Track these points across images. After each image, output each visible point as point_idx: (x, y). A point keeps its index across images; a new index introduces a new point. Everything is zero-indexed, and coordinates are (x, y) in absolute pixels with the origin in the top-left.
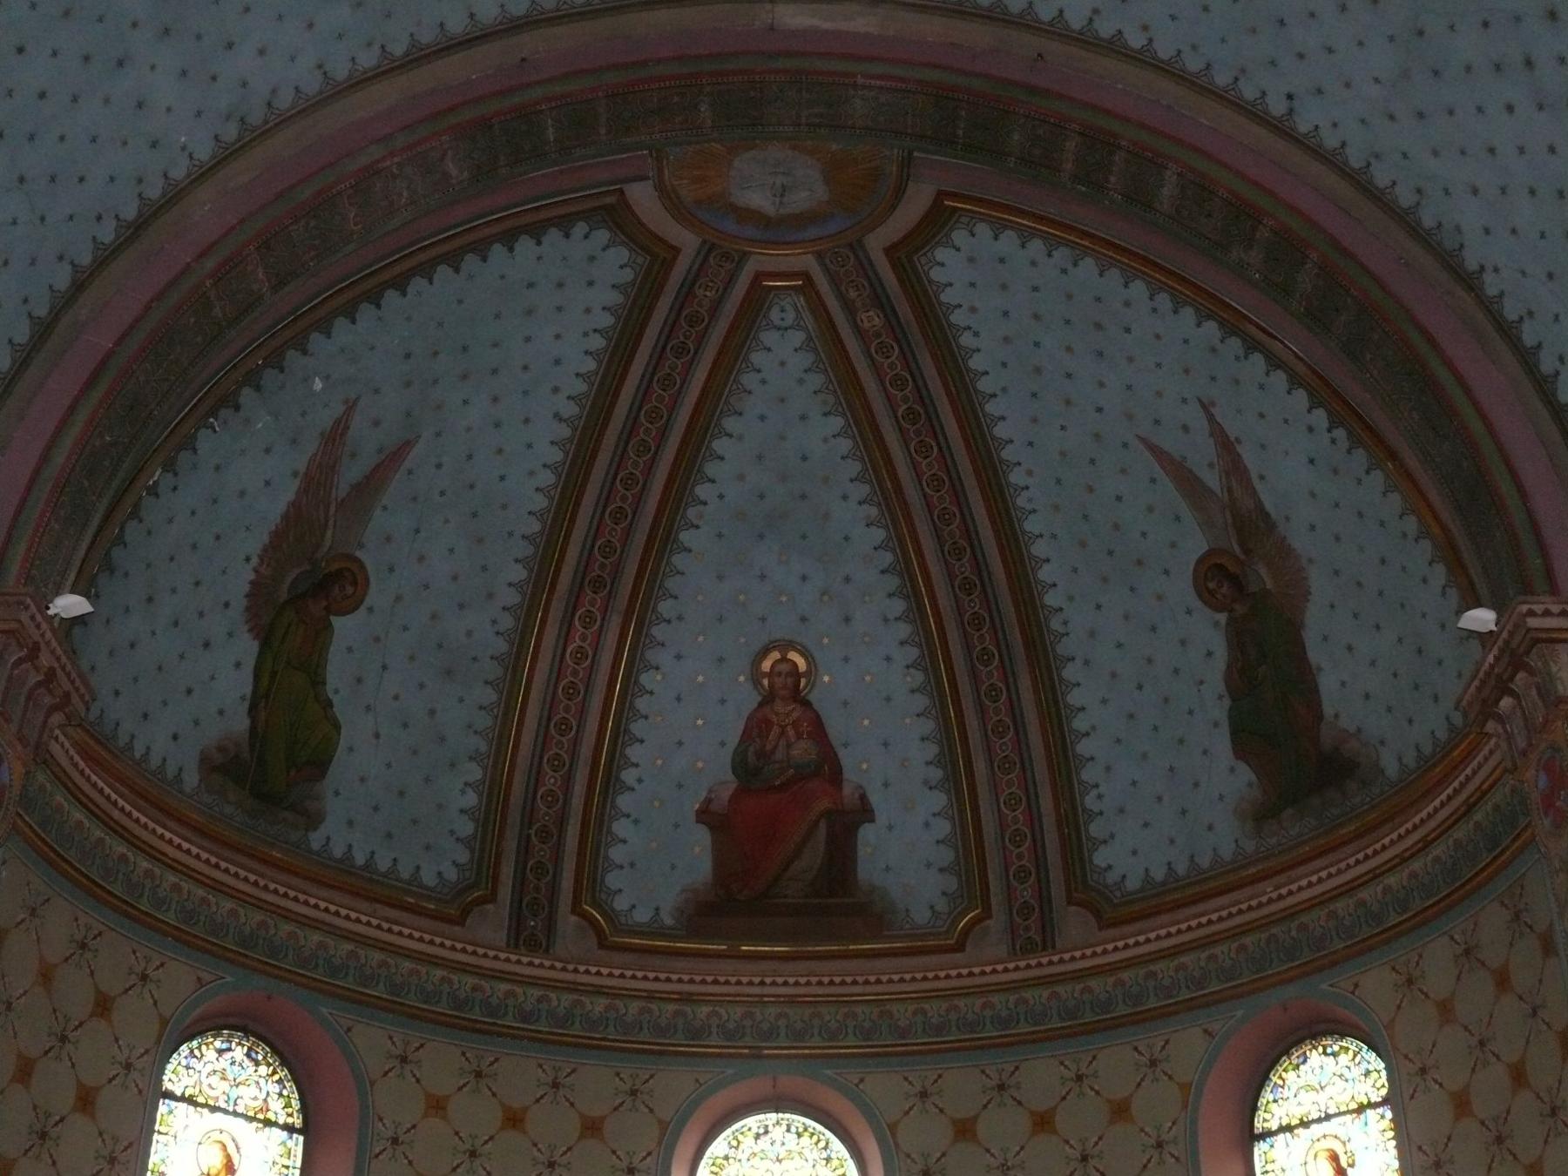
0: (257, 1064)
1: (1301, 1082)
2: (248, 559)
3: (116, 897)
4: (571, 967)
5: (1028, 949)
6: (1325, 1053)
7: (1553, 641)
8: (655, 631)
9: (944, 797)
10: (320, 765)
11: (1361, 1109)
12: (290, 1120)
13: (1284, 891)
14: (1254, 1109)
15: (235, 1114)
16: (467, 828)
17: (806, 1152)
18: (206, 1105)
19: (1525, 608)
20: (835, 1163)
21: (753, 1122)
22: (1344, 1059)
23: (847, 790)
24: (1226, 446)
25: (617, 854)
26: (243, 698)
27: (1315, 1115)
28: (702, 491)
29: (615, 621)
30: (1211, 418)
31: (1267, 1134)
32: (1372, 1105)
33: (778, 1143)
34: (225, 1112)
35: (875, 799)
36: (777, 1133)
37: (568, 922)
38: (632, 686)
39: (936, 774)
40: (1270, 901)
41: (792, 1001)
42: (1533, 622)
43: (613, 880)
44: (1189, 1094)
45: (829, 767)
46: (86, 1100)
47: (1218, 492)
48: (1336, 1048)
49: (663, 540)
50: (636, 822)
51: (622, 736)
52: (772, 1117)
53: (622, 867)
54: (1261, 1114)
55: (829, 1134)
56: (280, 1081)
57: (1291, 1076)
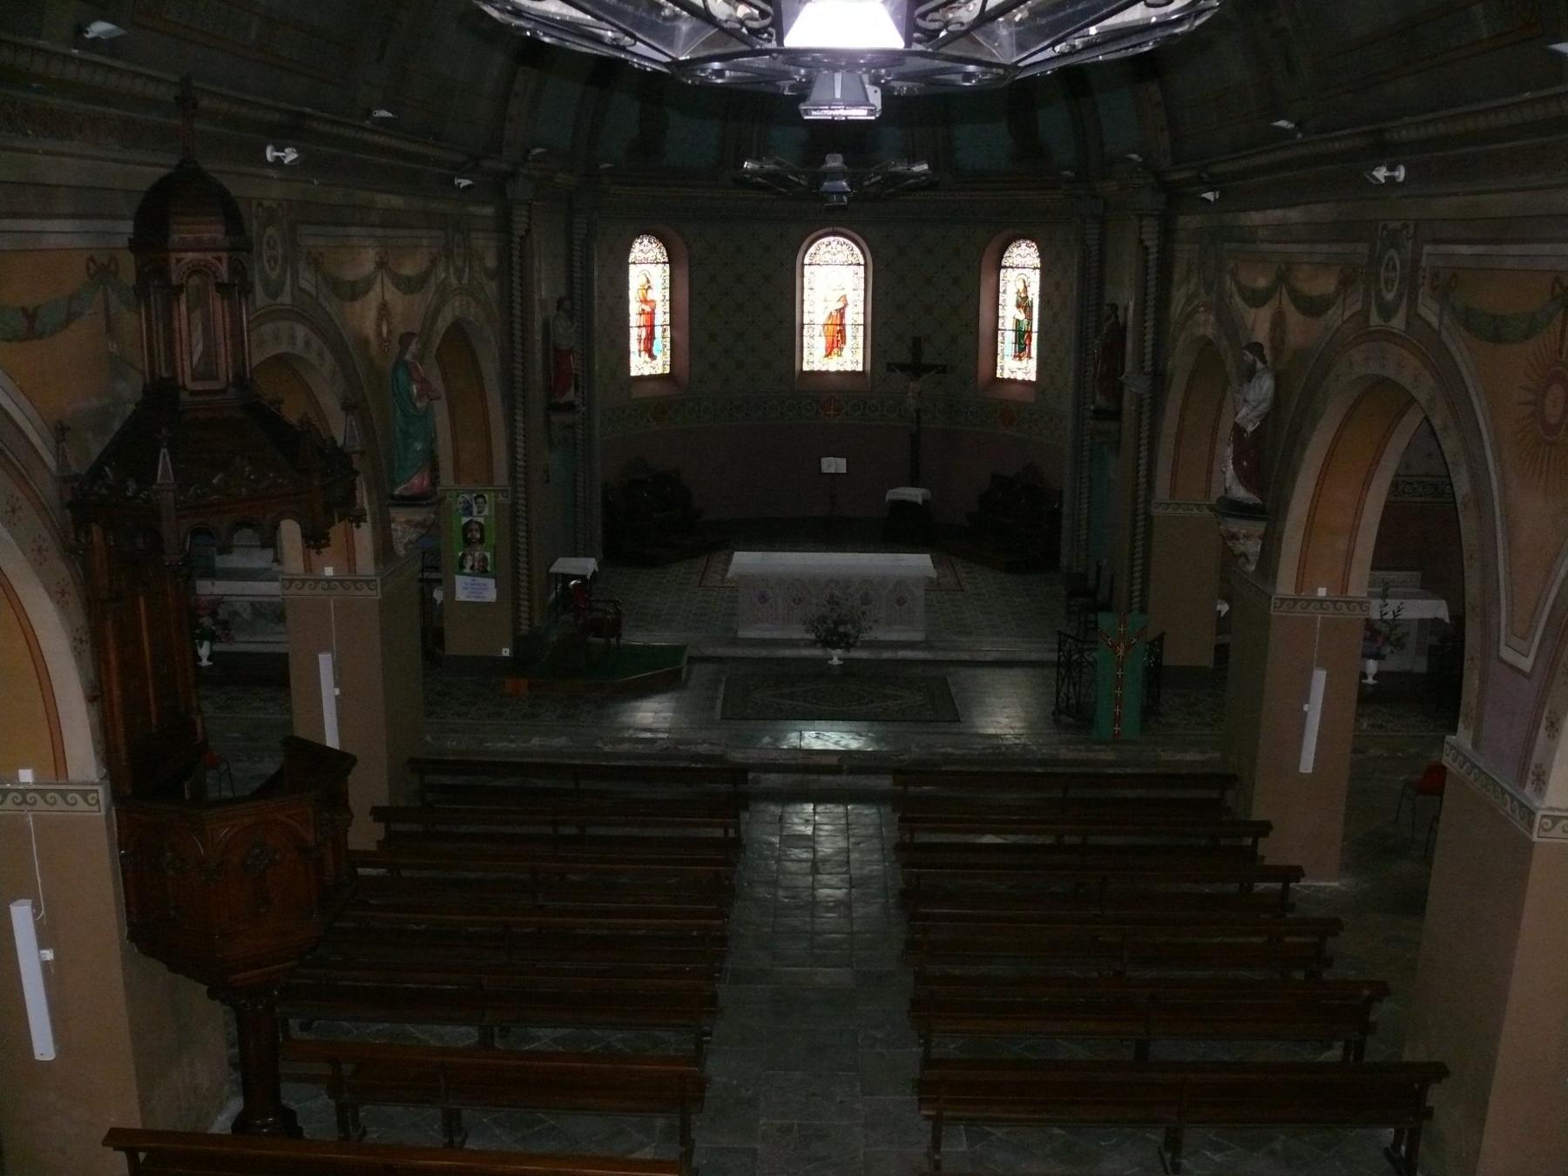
0: (651, 243)
1: (1019, 252)
20: (855, 256)
21: (825, 240)
31: (1005, 267)
56: (660, 248)
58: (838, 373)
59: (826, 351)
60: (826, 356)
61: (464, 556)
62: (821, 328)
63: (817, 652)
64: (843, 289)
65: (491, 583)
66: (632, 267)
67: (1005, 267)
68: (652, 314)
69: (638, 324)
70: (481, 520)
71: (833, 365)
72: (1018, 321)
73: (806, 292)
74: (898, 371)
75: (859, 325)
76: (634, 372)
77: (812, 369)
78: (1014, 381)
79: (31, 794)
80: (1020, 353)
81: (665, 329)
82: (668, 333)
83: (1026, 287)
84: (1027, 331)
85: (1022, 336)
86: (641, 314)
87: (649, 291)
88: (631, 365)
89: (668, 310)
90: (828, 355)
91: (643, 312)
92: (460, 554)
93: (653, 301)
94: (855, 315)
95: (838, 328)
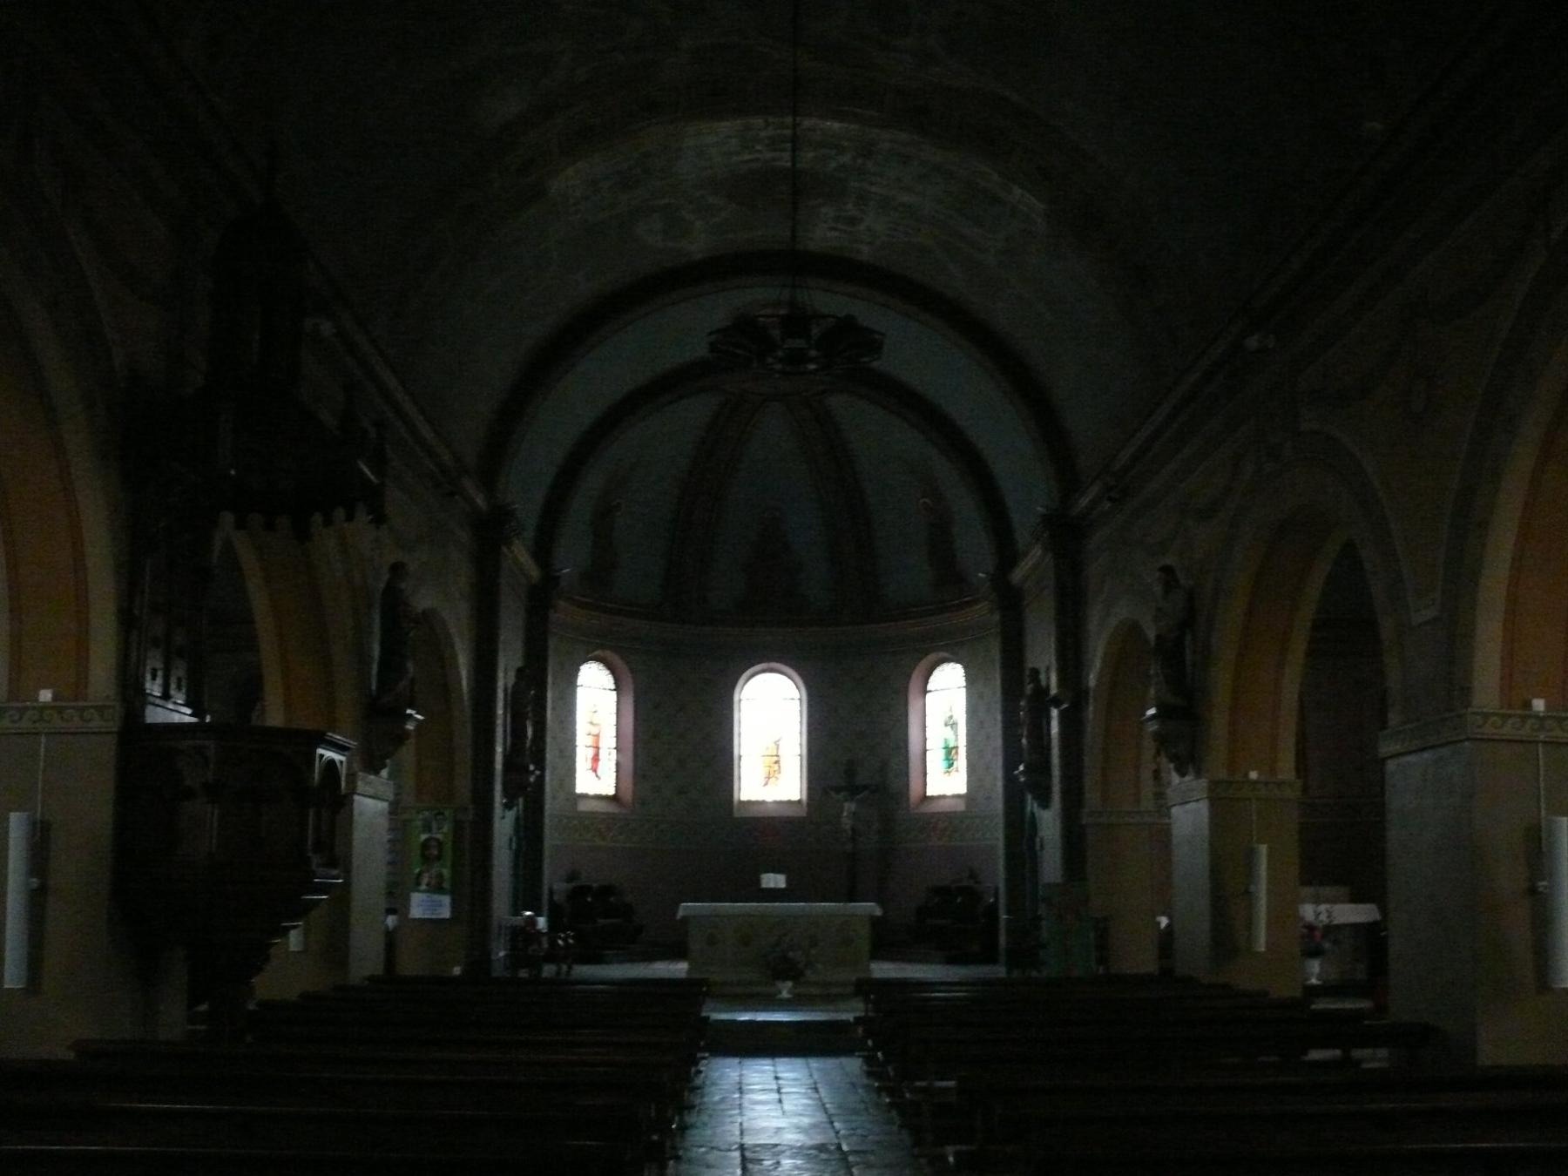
31: (930, 691)
61: (420, 874)
65: (446, 900)
67: (930, 691)
70: (439, 836)
79: (48, 712)
85: (950, 752)
88: (578, 743)
92: (417, 871)
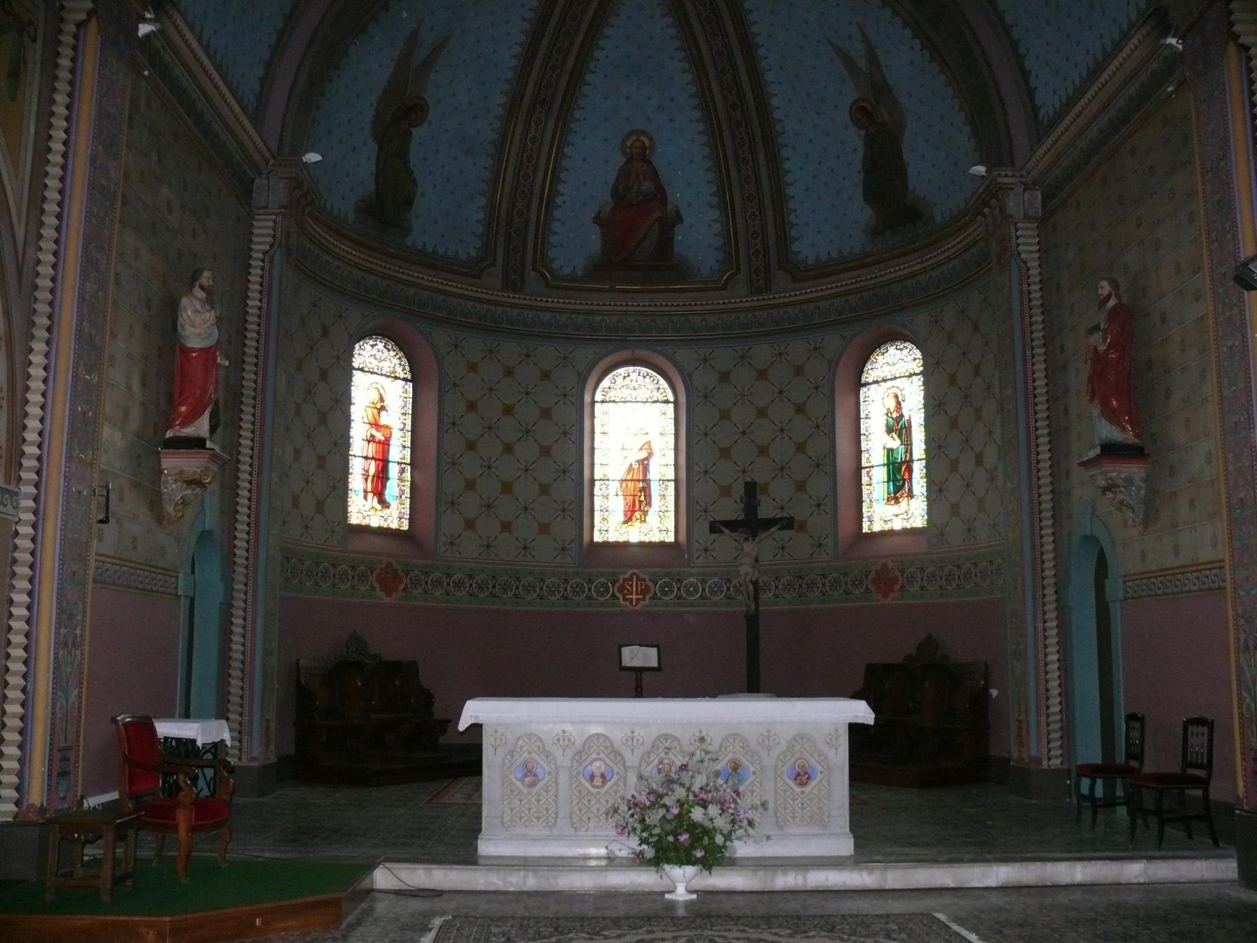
0: (389, 350)
1: (885, 361)
2: (372, 105)
3: (327, 280)
4: (533, 298)
5: (758, 291)
6: (897, 349)
7: (1008, 189)
8: (572, 126)
9: (718, 212)
10: (409, 203)
11: (911, 375)
12: (406, 376)
13: (883, 273)
14: (862, 372)
15: (382, 375)
16: (480, 229)
17: (648, 386)
18: (369, 372)
19: (996, 173)
20: (662, 391)
21: (622, 371)
22: (905, 352)
23: (669, 207)
24: (871, 50)
25: (554, 240)
26: (372, 174)
27: (889, 377)
28: (597, 54)
29: (551, 125)
30: (863, 34)
31: (867, 384)
32: (915, 374)
33: (634, 381)
34: (377, 374)
35: (684, 213)
36: (634, 376)
37: (531, 275)
38: (560, 154)
39: (715, 200)
40: (876, 277)
41: (641, 313)
42: (1000, 180)
43: (552, 253)
44: (832, 365)
45: (660, 195)
46: (324, 375)
47: (864, 69)
48: (902, 347)
49: (577, 79)
50: (563, 223)
51: (556, 180)
52: (631, 369)
53: (556, 246)
54: (864, 375)
55: (659, 377)
56: (400, 358)
57: (880, 358)
58: (642, 545)
59: (625, 515)
60: (626, 522)
62: (617, 484)
63: (645, 879)
64: (647, 434)
66: (357, 376)
67: (867, 384)
68: (385, 445)
69: (365, 455)
71: (635, 534)
72: (890, 452)
73: (598, 437)
74: (726, 531)
75: (668, 481)
76: (354, 519)
77: (605, 539)
78: (891, 533)
80: (895, 494)
81: (403, 469)
82: (408, 475)
83: (898, 403)
84: (906, 461)
85: (898, 473)
86: (369, 442)
87: (383, 413)
89: (409, 444)
90: (628, 520)
91: (371, 440)
93: (387, 427)
94: (663, 467)
95: (641, 485)
